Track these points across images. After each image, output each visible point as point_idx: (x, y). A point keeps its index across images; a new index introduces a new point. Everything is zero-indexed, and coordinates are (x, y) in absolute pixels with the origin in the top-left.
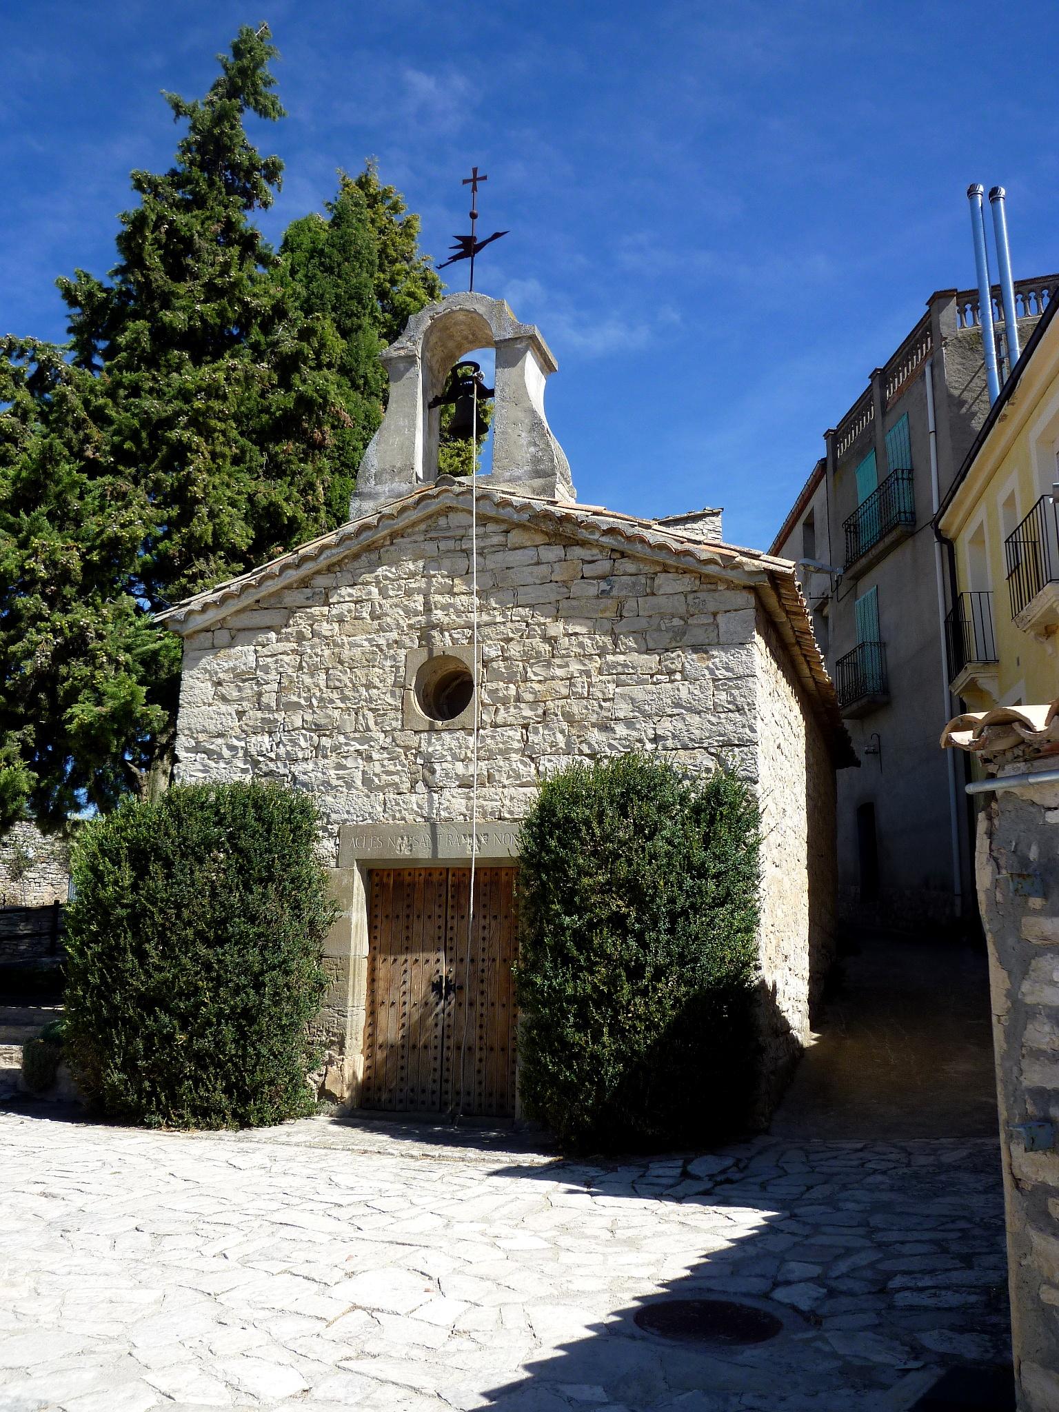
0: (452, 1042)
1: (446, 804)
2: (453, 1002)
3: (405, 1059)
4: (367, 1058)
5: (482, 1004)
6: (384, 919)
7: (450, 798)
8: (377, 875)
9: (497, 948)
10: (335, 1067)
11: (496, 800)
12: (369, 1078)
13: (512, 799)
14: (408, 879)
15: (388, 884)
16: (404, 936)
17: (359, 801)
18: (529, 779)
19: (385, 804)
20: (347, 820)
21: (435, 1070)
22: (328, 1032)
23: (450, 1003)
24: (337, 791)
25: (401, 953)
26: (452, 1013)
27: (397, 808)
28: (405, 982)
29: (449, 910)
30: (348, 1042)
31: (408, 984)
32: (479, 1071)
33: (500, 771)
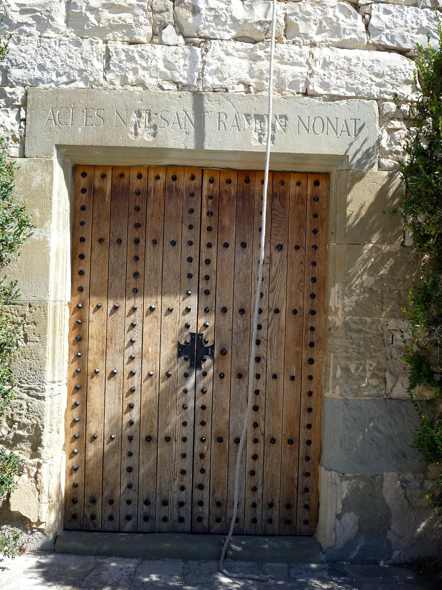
0: (206, 431)
1: (214, 64)
2: (211, 372)
3: (135, 457)
4: (72, 454)
5: (258, 376)
6: (96, 244)
7: (223, 55)
8: (84, 175)
9: (283, 294)
10: (25, 477)
11: (300, 65)
12: (75, 486)
13: (326, 64)
14: (136, 184)
15: (102, 191)
16: (130, 275)
17: (62, 50)
18: (354, 36)
19: (108, 57)
20: (37, 81)
21: (183, 472)
22: (11, 422)
23: (205, 374)
24: (21, 32)
25: (126, 296)
26: (210, 389)
27: (129, 65)
28: (132, 342)
29: (204, 234)
30: (46, 438)
31: (137, 346)
32: (253, 473)
33: (306, 20)
